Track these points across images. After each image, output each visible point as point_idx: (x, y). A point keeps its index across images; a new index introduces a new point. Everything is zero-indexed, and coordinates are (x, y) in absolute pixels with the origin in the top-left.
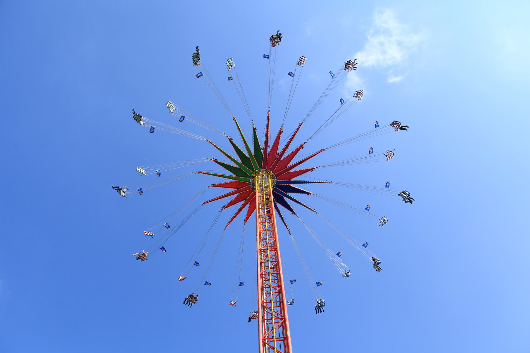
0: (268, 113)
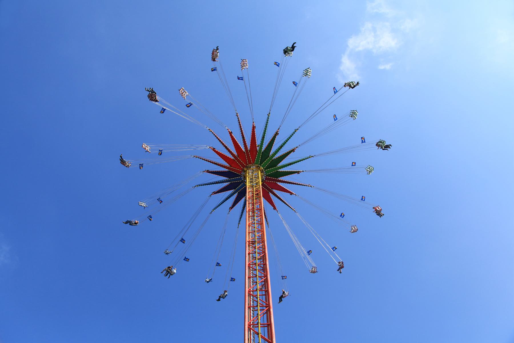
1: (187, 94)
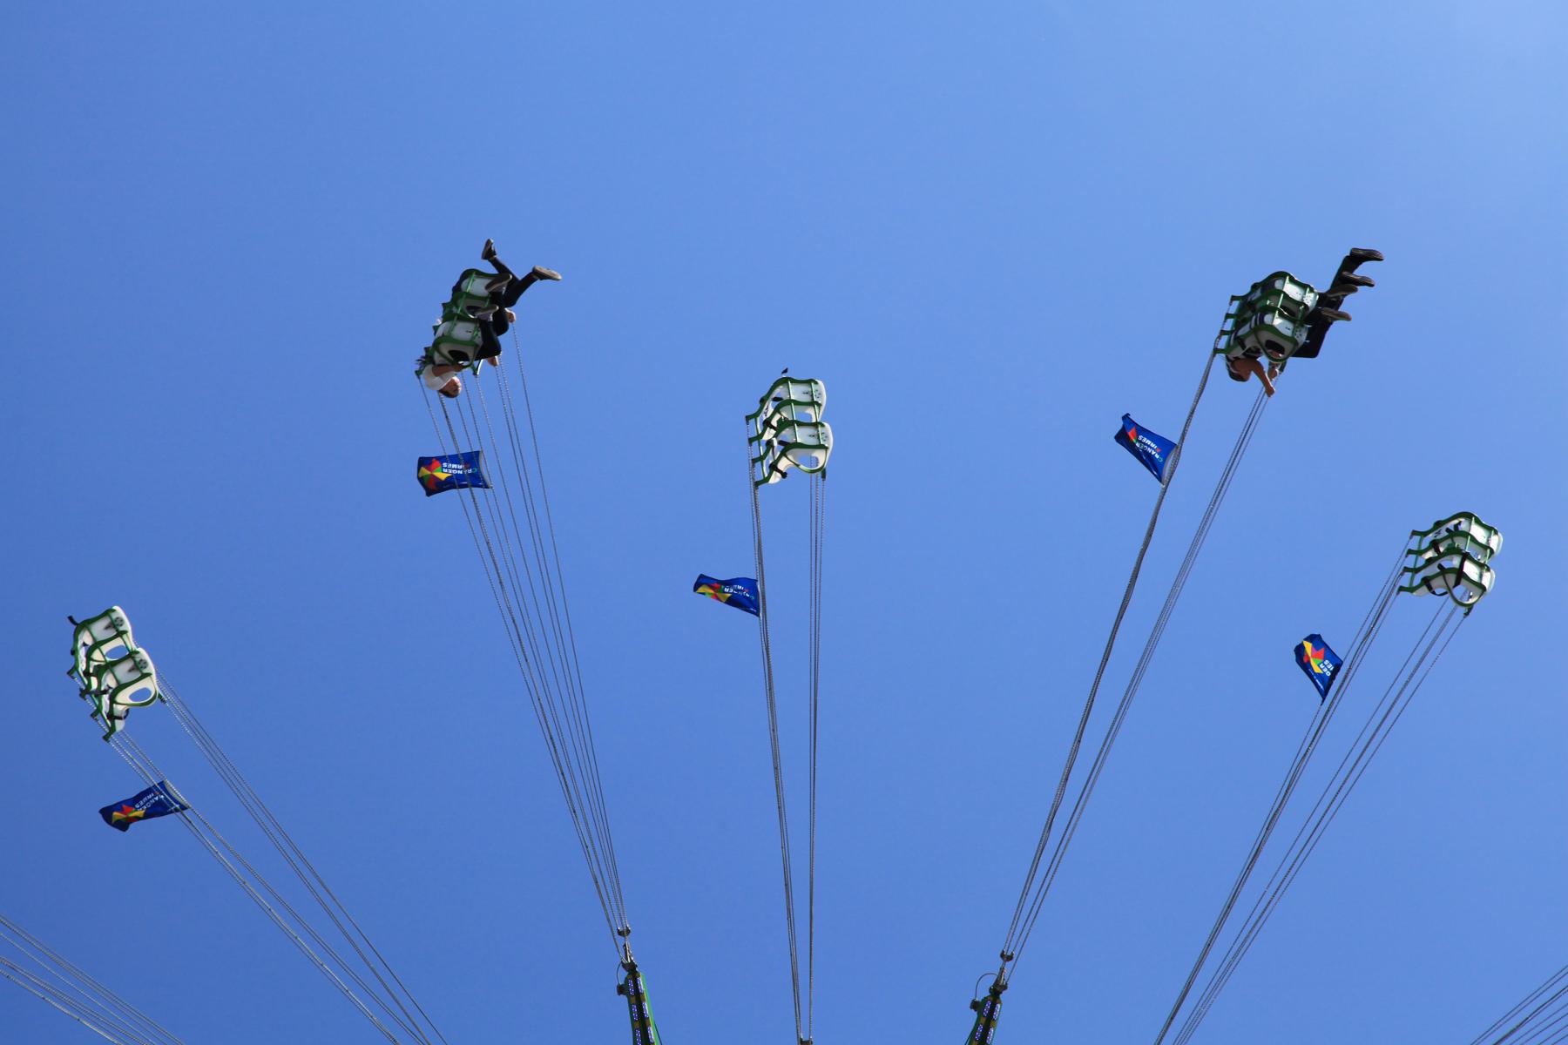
0: (630, 990)
1: (151, 685)
